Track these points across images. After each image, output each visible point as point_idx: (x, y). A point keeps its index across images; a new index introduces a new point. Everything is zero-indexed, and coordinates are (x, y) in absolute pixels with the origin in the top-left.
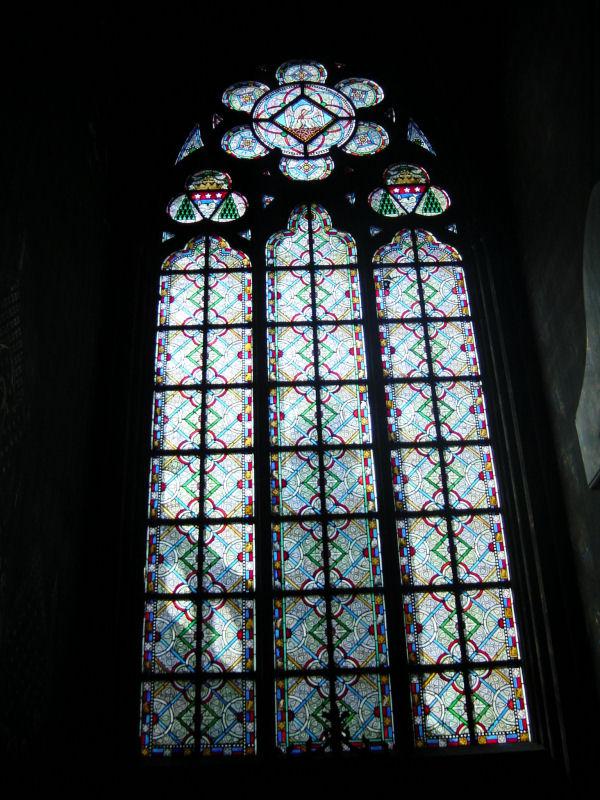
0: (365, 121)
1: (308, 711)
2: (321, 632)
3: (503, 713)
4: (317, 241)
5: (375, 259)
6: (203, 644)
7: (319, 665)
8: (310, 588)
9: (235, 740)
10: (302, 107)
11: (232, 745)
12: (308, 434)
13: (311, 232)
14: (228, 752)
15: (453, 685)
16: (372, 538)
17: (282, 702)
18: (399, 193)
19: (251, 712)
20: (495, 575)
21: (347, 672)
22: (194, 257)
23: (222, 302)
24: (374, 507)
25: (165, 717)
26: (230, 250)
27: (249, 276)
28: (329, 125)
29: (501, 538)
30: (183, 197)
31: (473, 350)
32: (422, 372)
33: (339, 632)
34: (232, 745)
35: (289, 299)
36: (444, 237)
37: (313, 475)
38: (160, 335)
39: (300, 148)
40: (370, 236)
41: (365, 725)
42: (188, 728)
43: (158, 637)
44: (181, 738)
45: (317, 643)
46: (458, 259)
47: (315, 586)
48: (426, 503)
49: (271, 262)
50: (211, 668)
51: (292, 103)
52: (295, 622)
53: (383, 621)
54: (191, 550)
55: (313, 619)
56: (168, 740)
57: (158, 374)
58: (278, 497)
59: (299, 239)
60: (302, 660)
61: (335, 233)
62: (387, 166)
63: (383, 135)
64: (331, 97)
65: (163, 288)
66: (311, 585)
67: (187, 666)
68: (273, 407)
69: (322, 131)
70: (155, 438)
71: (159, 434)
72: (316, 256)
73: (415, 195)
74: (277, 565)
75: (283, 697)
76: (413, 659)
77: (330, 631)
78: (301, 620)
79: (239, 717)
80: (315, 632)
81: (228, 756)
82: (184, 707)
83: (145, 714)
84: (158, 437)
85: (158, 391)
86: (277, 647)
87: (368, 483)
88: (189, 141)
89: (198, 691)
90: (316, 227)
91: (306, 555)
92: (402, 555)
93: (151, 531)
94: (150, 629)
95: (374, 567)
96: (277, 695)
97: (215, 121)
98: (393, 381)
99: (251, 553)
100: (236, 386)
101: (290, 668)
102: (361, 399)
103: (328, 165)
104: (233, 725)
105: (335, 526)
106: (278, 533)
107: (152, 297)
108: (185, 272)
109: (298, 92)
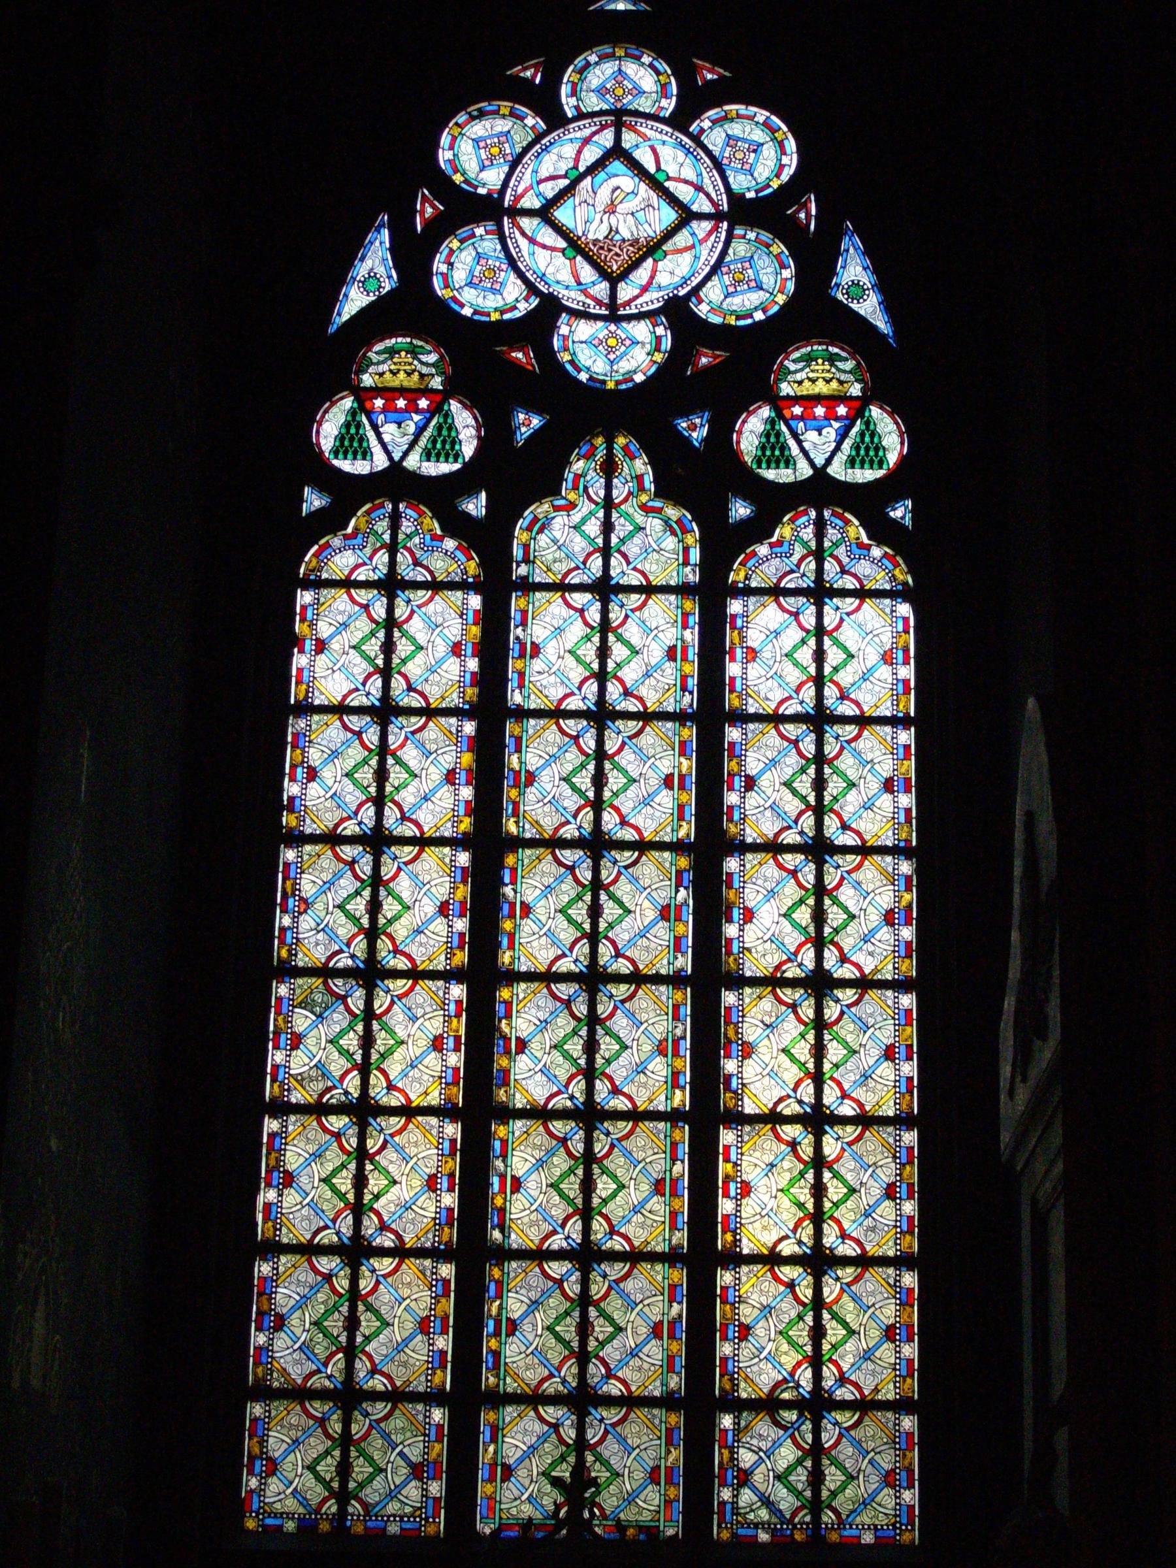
0: (751, 224)
1: (537, 1465)
2: (568, 1329)
3: (872, 1487)
4: (621, 527)
5: (736, 576)
6: (359, 1339)
7: (561, 1388)
8: (555, 1247)
9: (408, 1510)
10: (614, 182)
11: (402, 1518)
12: (571, 949)
13: (609, 504)
14: (393, 1529)
15: (792, 1437)
16: (674, 1159)
17: (491, 1449)
18: (801, 418)
19: (437, 1463)
20: (891, 1243)
21: (609, 1401)
22: (368, 551)
23: (420, 658)
24: (683, 1101)
25: (287, 1466)
26: (441, 539)
27: (458, 991)
28: (670, 234)
29: (911, 1175)
30: (348, 403)
31: (907, 790)
32: (801, 833)
33: (601, 1329)
34: (402, 1518)
35: (553, 659)
36: (882, 530)
37: (575, 1032)
38: (305, 597)
39: (601, 289)
40: (725, 508)
41: (630, 1499)
42: (327, 1484)
43: (280, 1323)
44: (314, 1503)
45: (560, 1347)
46: (905, 584)
47: (564, 1244)
48: (781, 1100)
49: (523, 570)
50: (370, 1383)
51: (592, 170)
52: (525, 1307)
53: (680, 1316)
54: (343, 1166)
55: (556, 1303)
56: (291, 1505)
57: (291, 808)
58: (506, 1072)
59: (584, 521)
60: (531, 1377)
61: (659, 510)
62: (783, 348)
63: (783, 266)
64: (681, 155)
65: (303, 620)
66: (557, 1243)
67: (329, 1377)
68: (508, 890)
69: (653, 248)
70: (282, 942)
71: (289, 934)
72: (616, 561)
73: (836, 425)
74: (499, 1201)
75: (494, 1439)
76: (728, 1387)
77: (584, 1328)
78: (535, 1304)
80: (558, 1328)
81: (394, 1536)
82: (321, 1449)
83: (252, 1458)
84: (289, 940)
85: (289, 845)
86: (490, 1350)
87: (676, 1053)
88: (362, 259)
89: (347, 1422)
90: (619, 491)
91: (552, 1185)
92: (726, 1195)
93: (271, 1125)
94: (289, 890)
95: (674, 1215)
96: (485, 1435)
97: (422, 212)
98: (743, 848)
99: (451, 1176)
100: (441, 842)
101: (509, 1390)
102: (679, 884)
103: (658, 339)
104: (405, 1484)
105: (608, 1134)
106: (504, 1143)
107: (276, 638)
108: (347, 584)
109: (606, 139)
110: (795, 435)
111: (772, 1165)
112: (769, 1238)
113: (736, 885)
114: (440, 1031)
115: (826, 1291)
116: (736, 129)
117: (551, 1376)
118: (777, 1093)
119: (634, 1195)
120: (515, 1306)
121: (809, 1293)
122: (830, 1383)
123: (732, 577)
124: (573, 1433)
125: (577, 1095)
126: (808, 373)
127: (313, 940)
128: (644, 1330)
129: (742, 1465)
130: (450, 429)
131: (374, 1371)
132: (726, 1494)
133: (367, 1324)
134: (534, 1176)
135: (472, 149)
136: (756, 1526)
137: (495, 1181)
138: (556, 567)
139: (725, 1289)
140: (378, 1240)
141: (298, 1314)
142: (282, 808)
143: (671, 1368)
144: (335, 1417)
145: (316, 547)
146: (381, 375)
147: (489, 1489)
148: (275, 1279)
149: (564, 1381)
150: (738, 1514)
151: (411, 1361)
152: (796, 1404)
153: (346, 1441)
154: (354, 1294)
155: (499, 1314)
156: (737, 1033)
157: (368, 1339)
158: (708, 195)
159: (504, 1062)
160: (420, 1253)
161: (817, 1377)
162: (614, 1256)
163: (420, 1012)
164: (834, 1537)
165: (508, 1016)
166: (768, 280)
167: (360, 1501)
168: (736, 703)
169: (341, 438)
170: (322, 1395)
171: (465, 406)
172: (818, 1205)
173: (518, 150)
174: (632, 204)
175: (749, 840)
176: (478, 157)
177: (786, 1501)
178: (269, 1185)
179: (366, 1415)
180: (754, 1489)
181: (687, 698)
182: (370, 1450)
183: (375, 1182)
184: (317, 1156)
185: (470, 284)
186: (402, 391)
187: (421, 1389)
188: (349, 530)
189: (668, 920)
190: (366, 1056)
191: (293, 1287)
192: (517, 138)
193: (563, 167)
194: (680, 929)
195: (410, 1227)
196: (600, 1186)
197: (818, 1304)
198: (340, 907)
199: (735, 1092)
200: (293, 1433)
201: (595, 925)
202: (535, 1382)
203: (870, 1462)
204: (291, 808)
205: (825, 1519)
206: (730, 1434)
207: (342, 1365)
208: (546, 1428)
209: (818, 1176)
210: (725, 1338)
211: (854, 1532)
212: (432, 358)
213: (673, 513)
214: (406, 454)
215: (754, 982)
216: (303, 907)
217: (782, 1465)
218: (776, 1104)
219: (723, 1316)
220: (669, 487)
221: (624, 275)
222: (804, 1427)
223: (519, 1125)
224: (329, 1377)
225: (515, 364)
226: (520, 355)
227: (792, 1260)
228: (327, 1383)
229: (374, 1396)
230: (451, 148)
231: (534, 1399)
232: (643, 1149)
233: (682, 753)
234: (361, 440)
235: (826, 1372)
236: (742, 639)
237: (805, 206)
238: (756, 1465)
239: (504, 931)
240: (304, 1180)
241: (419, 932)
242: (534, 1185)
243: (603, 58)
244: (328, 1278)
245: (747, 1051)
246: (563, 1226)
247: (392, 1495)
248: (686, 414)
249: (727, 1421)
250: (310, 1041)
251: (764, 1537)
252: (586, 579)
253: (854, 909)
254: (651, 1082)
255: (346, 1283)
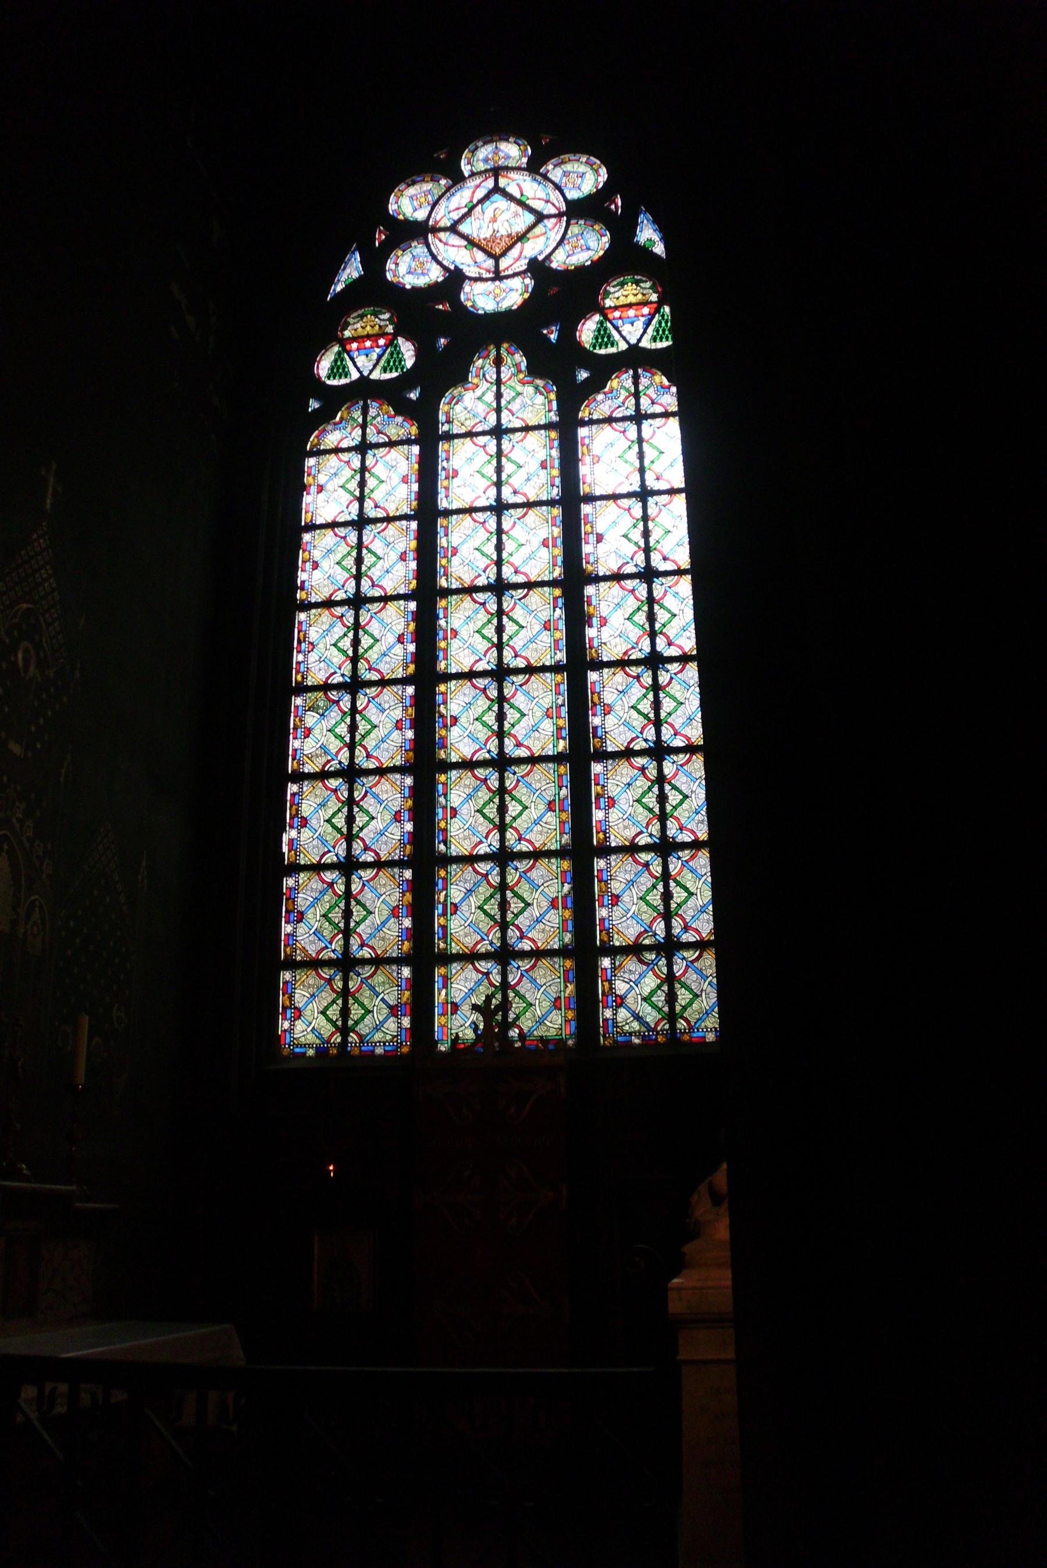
2: (493, 907)
5: (584, 414)
6: (352, 924)
7: (489, 948)
8: (482, 852)
9: (388, 1037)
10: (495, 206)
11: (384, 1043)
14: (379, 1051)
17: (444, 992)
21: (523, 955)
25: (307, 1012)
30: (336, 349)
32: (636, 565)
33: (515, 905)
34: (384, 1043)
38: (311, 462)
39: (490, 263)
40: (575, 380)
41: (540, 1021)
43: (301, 917)
44: (326, 1036)
48: (633, 740)
49: (446, 428)
51: (481, 201)
52: (463, 895)
55: (484, 890)
56: (311, 1038)
57: (302, 588)
58: (444, 739)
59: (483, 394)
60: (469, 941)
65: (309, 475)
67: (333, 951)
69: (521, 237)
74: (443, 825)
75: (445, 986)
77: (504, 906)
78: (469, 892)
79: (394, 1011)
80: (485, 907)
81: (380, 1056)
84: (302, 669)
86: (440, 925)
88: (344, 269)
89: (346, 980)
91: (478, 811)
93: (293, 788)
94: (302, 638)
105: (515, 773)
108: (337, 451)
109: (490, 183)
110: (617, 328)
111: (629, 784)
112: (630, 833)
113: (594, 602)
114: (400, 717)
115: (671, 867)
116: (568, 167)
117: (483, 939)
118: (630, 735)
119: (534, 813)
120: (456, 894)
121: (660, 869)
122: (677, 931)
123: (580, 415)
124: (499, 978)
125: (493, 749)
126: (622, 293)
127: (317, 668)
128: (545, 904)
129: (618, 993)
130: (398, 354)
131: (363, 945)
132: (608, 1013)
133: (357, 912)
134: (466, 806)
135: (408, 203)
136: (631, 1034)
137: (440, 811)
138: (467, 423)
139: (600, 871)
140: (363, 857)
141: (312, 910)
142: (297, 588)
143: (565, 930)
144: (338, 977)
145: (317, 432)
146: (356, 330)
147: (443, 1020)
148: (296, 889)
149: (491, 943)
150: (617, 1027)
151: (387, 936)
152: (654, 948)
153: (345, 993)
154: (348, 894)
155: (446, 900)
156: (600, 698)
157: (358, 924)
158: (553, 205)
159: (443, 732)
160: (391, 864)
161: (668, 927)
162: (522, 856)
163: (386, 706)
164: (686, 1037)
165: (445, 702)
166: (593, 244)
167: (357, 1033)
168: (587, 490)
169: (332, 369)
170: (329, 963)
171: (407, 340)
172: (662, 809)
173: (436, 197)
174: (507, 215)
175: (601, 574)
176: (412, 205)
177: (651, 1016)
178: (292, 827)
179: (359, 975)
180: (628, 1009)
181: (562, 743)
182: (361, 999)
183: (360, 819)
184: (323, 805)
185: (409, 273)
186: (368, 337)
187: (394, 955)
188: (338, 419)
189: (549, 630)
190: (352, 738)
191: (308, 893)
192: (435, 191)
193: (464, 203)
194: (558, 635)
195: (384, 847)
196: (510, 808)
197: (666, 876)
198: (335, 645)
199: (601, 738)
200: (311, 990)
201: (500, 638)
202: (471, 945)
203: (709, 984)
204: (302, 588)
205: (679, 1026)
206: (609, 971)
207: (341, 942)
208: (480, 976)
209: (661, 789)
210: (602, 905)
211: (701, 1034)
212: (387, 316)
213: (540, 382)
214: (371, 371)
215: (610, 664)
216: (311, 647)
217: (646, 991)
218: (629, 743)
219: (600, 890)
220: (535, 370)
221: (504, 254)
222: (660, 963)
223: (454, 774)
224: (333, 951)
225: (439, 310)
226: (441, 307)
227: (647, 848)
228: (332, 955)
229: (364, 962)
230: (396, 203)
231: (471, 957)
232: (539, 781)
233: (554, 525)
234: (344, 368)
235: (674, 923)
236: (589, 450)
237: (614, 202)
238: (629, 991)
239: (440, 649)
240: (314, 822)
241: (385, 655)
242: (467, 811)
243: (485, 143)
244: (331, 885)
245: (608, 710)
246: (486, 837)
247: (377, 1028)
248: (547, 327)
249: (606, 962)
250: (316, 732)
251: (636, 1041)
252: (487, 428)
253: (675, 611)
254: (542, 736)
255: (343, 888)
